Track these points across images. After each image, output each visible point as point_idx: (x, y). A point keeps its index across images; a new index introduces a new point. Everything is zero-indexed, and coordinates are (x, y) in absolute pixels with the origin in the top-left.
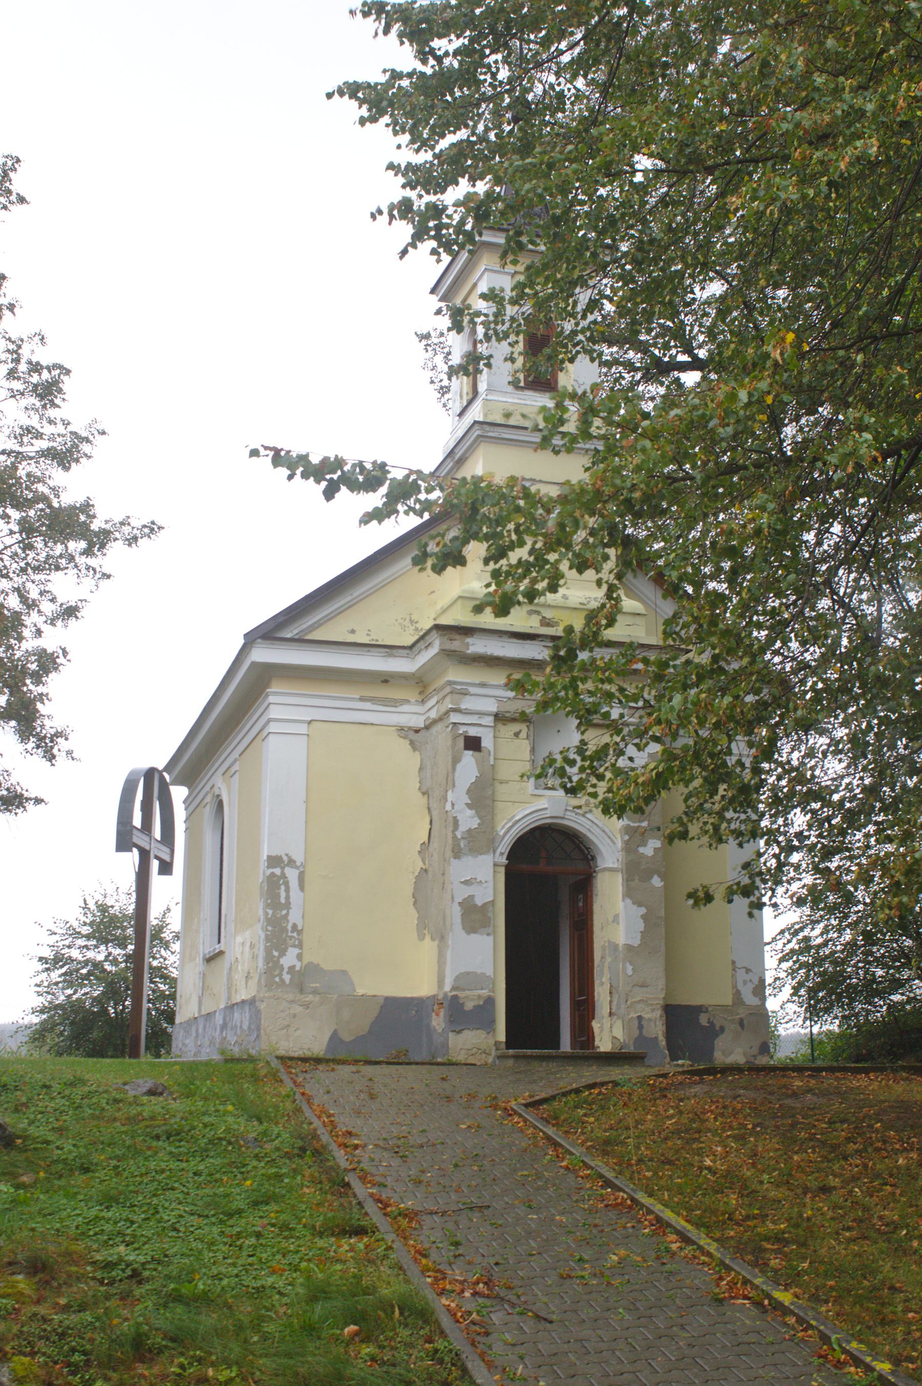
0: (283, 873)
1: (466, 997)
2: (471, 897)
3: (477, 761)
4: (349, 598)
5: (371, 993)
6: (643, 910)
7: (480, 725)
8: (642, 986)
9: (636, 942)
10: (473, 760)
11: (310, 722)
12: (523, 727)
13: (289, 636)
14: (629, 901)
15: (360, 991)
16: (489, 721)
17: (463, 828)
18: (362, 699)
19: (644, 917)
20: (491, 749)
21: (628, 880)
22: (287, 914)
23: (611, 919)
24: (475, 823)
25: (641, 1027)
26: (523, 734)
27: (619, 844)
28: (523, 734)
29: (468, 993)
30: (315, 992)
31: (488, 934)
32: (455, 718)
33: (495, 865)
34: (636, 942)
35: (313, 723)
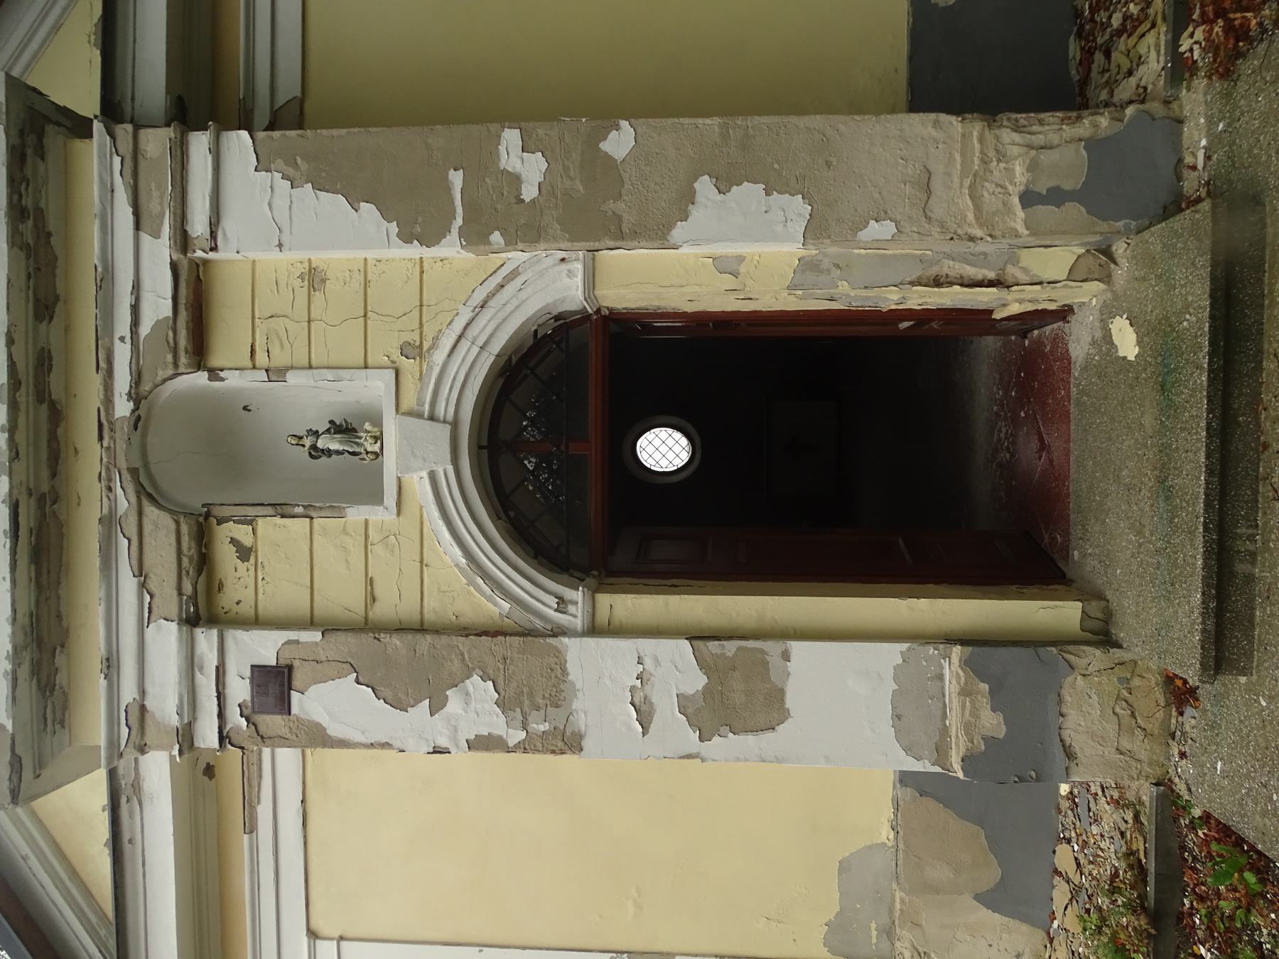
1: (968, 728)
2: (684, 703)
4: (34, 862)
5: (889, 812)
6: (704, 186)
7: (220, 672)
8: (928, 191)
9: (798, 207)
10: (314, 691)
11: (313, 934)
12: (226, 533)
14: (679, 231)
15: (885, 834)
16: (206, 640)
17: (496, 723)
18: (251, 827)
19: (724, 185)
20: (281, 637)
21: (621, 235)
23: (728, 281)
24: (482, 690)
25: (1056, 197)
26: (242, 533)
27: (516, 257)
28: (242, 533)
29: (953, 721)
30: (889, 933)
31: (786, 656)
32: (208, 736)
33: (593, 630)
34: (798, 207)
35: (315, 924)
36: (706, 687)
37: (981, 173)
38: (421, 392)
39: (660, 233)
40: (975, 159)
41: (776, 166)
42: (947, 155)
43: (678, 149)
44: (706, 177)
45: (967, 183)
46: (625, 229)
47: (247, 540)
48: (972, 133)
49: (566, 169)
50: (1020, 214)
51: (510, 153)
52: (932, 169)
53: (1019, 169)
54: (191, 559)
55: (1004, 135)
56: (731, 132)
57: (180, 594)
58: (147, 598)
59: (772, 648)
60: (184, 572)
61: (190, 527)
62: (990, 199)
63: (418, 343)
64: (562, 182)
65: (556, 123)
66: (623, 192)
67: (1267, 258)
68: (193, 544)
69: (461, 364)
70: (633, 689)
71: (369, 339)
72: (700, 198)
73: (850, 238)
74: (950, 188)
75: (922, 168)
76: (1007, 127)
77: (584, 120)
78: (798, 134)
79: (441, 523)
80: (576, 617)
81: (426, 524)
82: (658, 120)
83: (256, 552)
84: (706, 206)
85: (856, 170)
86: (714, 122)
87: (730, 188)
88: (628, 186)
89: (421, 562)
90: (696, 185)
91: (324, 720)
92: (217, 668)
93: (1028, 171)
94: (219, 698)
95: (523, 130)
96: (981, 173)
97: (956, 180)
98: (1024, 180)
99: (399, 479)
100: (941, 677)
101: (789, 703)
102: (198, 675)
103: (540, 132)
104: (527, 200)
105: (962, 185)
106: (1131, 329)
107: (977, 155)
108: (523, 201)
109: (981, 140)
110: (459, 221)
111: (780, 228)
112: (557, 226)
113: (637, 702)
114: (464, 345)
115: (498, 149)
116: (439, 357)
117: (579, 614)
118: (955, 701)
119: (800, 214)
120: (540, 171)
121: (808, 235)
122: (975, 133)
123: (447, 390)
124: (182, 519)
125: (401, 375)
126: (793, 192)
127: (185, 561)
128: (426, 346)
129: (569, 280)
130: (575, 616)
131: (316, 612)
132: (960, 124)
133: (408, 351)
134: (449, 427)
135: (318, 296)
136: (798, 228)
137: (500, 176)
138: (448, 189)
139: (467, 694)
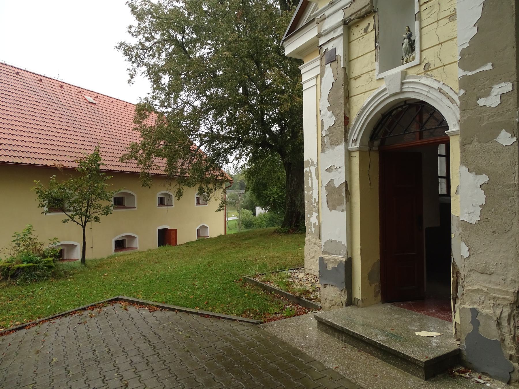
0: (310, 170)
1: (328, 260)
2: (331, 181)
3: (127, 105)
6: (484, 179)
9: (475, 218)
13: (304, 24)
14: (465, 169)
22: (312, 193)
25: (475, 323)
29: (331, 257)
31: (343, 211)
36: (335, 187)
37: (488, 296)
38: (413, 77)
39: (464, 161)
40: (496, 295)
41: (493, 209)
42: (499, 283)
43: (502, 165)
44: (488, 179)
45: (485, 289)
46: (465, 147)
47: (369, 30)
48: (509, 295)
49: (493, 116)
50: (468, 307)
51: (500, 89)
52: (492, 276)
53: (489, 311)
54: (360, 14)
55: (507, 309)
56: (510, 189)
57: (351, 16)
58: (348, 6)
59: (344, 207)
60: (356, 14)
61: (368, 9)
62: (477, 297)
63: (430, 69)
64: (487, 115)
65: (516, 106)
66: (482, 143)
67: (408, 374)
68: (364, 13)
69: (420, 89)
70: (334, 166)
71: (432, 48)
72: (479, 177)
73: (462, 239)
74: (484, 282)
75: (492, 272)
76: (512, 311)
77: (517, 120)
78: (509, 220)
79: (372, 96)
80: (352, 147)
81: (375, 90)
82: (517, 155)
83: (367, 34)
84: (475, 180)
85: (492, 244)
86: (516, 181)
87: (483, 190)
88: (485, 145)
89: (365, 92)
90: (484, 175)
91: (325, 76)
92: (334, 38)
93: (486, 314)
94: (328, 41)
95: (512, 92)
96: (488, 296)
97: (487, 285)
98: (483, 312)
99: (383, 78)
100: (340, 255)
101: (333, 211)
102: (332, 32)
103: (512, 100)
104: (478, 102)
105: (485, 287)
106: (426, 336)
107: (497, 296)
108: (478, 100)
109: (504, 299)
110: (469, 74)
111: (466, 211)
112: (467, 117)
113: (332, 167)
114: (426, 89)
115: (503, 82)
116: (424, 81)
117: (352, 147)
118: (334, 257)
119: (471, 219)
120: (491, 105)
121: (463, 222)
122: (508, 297)
123: (412, 87)
124: (370, 5)
125: (419, 66)
126: (481, 217)
127: (359, 13)
128: (429, 73)
129: (452, 124)
130: (352, 146)
131: (352, 61)
132: (513, 291)
133: (427, 67)
134: (399, 91)
135: (447, 20)
136: (466, 218)
137: (490, 86)
138: (484, 64)
139: (331, 117)
